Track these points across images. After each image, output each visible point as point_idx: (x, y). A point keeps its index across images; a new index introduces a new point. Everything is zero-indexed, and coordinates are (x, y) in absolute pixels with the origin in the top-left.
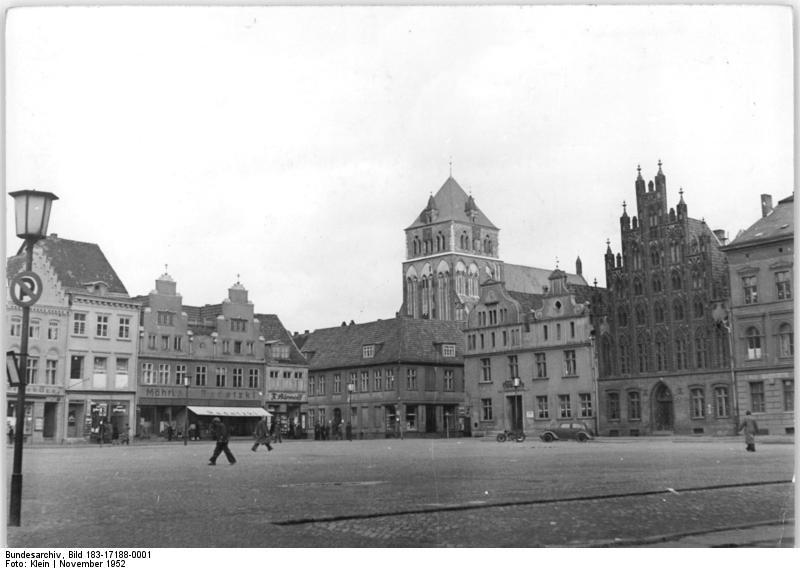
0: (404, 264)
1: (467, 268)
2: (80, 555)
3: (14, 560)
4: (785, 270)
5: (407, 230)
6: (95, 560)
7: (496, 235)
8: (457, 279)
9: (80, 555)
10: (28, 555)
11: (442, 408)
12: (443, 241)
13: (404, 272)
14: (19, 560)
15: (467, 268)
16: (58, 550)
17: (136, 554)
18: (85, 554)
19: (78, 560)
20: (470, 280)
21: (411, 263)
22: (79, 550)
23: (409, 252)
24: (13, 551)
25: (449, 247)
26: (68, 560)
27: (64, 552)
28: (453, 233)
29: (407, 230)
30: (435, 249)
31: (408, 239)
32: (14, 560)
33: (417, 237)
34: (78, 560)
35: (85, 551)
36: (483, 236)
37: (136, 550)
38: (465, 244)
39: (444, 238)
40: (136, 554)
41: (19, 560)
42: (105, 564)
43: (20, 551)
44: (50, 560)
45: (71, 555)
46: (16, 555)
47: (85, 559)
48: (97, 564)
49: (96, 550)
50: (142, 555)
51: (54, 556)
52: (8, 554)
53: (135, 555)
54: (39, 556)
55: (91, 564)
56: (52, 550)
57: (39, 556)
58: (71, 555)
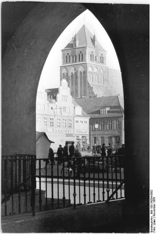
0: (61, 67)
1: (93, 70)
2: (152, 210)
3: (153, 230)
4: (85, 76)
5: (63, 51)
6: (153, 206)
7: (105, 54)
8: (88, 75)
9: (152, 210)
10: (152, 226)
11: (43, 160)
12: (82, 57)
13: (61, 71)
14: (153, 228)
15: (93, 70)
16: (150, 217)
17: (151, 194)
18: (152, 209)
19: (153, 211)
20: (94, 76)
21: (65, 67)
22: (150, 211)
23: (64, 61)
24: (150, 230)
25: (85, 59)
26: (153, 214)
27: (151, 215)
28: (87, 53)
29: (63, 51)
30: (78, 60)
31: (63, 55)
32: (153, 230)
33: (68, 54)
34: (153, 211)
35: (150, 209)
36: (100, 55)
37: (150, 194)
38: (92, 58)
39: (82, 55)
40: (151, 194)
41: (153, 228)
42: (154, 203)
43: (150, 228)
44: (153, 219)
45: (152, 213)
46: (152, 229)
47: (153, 209)
48: (154, 205)
49: (150, 206)
50: (152, 192)
51: (152, 218)
52: (151, 232)
53: (152, 194)
54: (152, 223)
55: (154, 207)
56: (150, 219)
57: (152, 223)
58: (152, 213)
